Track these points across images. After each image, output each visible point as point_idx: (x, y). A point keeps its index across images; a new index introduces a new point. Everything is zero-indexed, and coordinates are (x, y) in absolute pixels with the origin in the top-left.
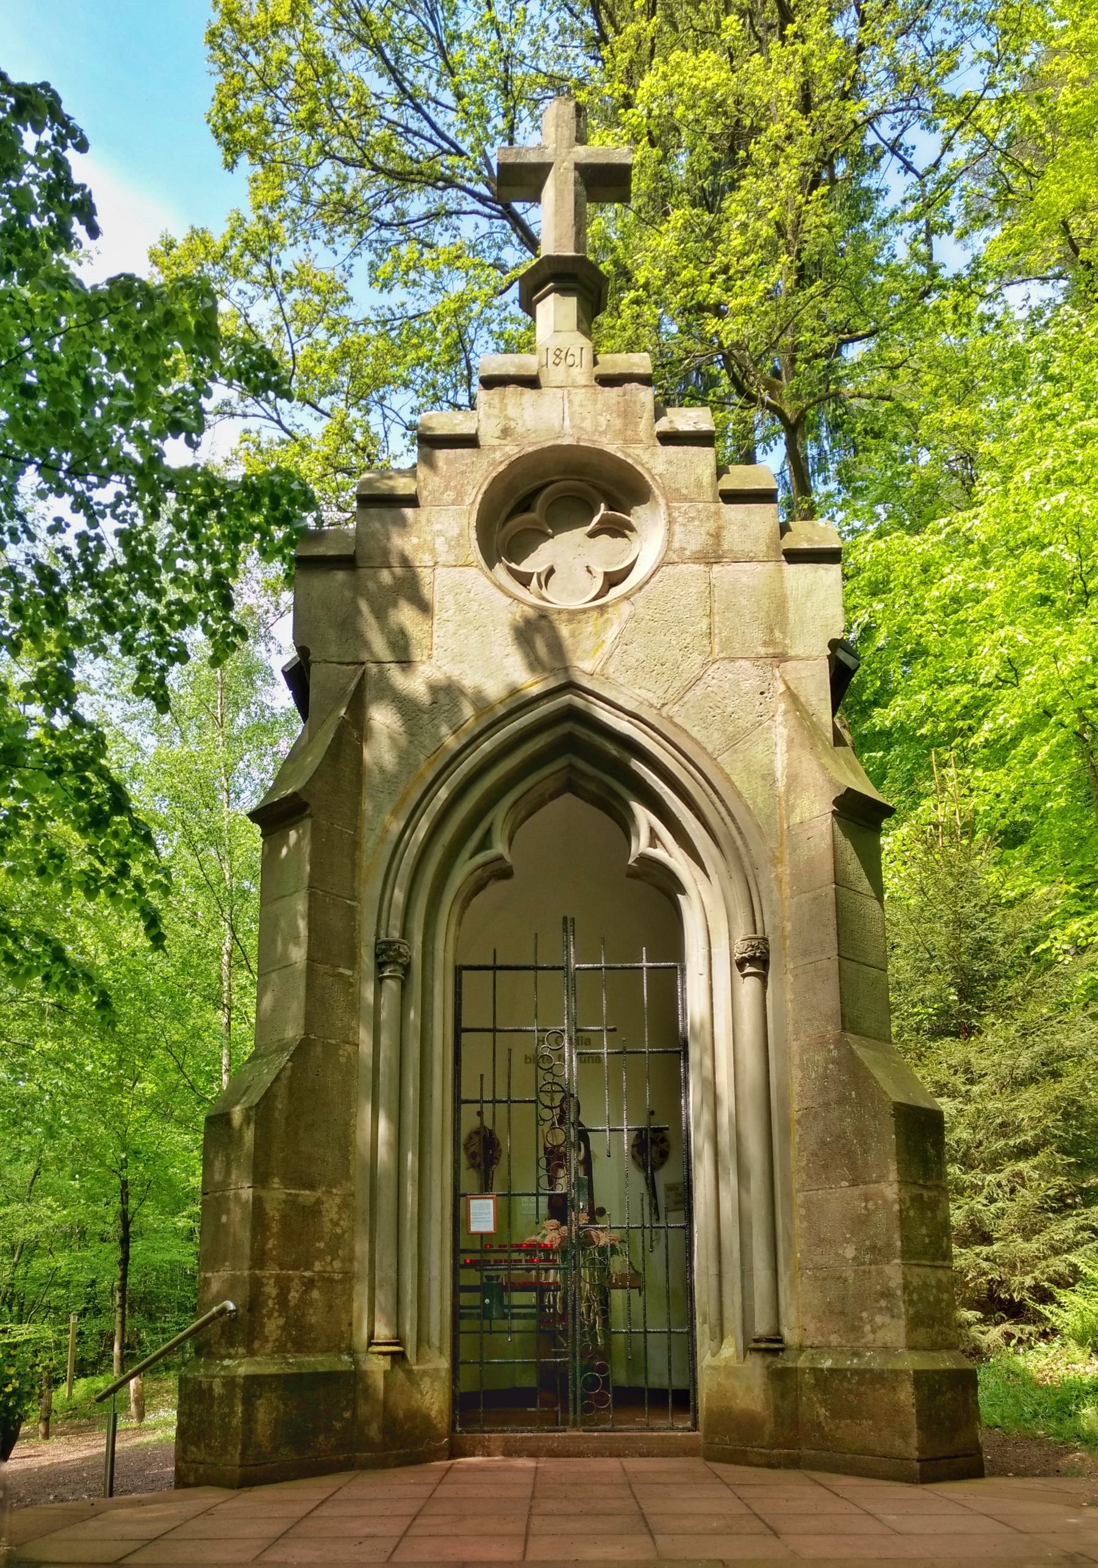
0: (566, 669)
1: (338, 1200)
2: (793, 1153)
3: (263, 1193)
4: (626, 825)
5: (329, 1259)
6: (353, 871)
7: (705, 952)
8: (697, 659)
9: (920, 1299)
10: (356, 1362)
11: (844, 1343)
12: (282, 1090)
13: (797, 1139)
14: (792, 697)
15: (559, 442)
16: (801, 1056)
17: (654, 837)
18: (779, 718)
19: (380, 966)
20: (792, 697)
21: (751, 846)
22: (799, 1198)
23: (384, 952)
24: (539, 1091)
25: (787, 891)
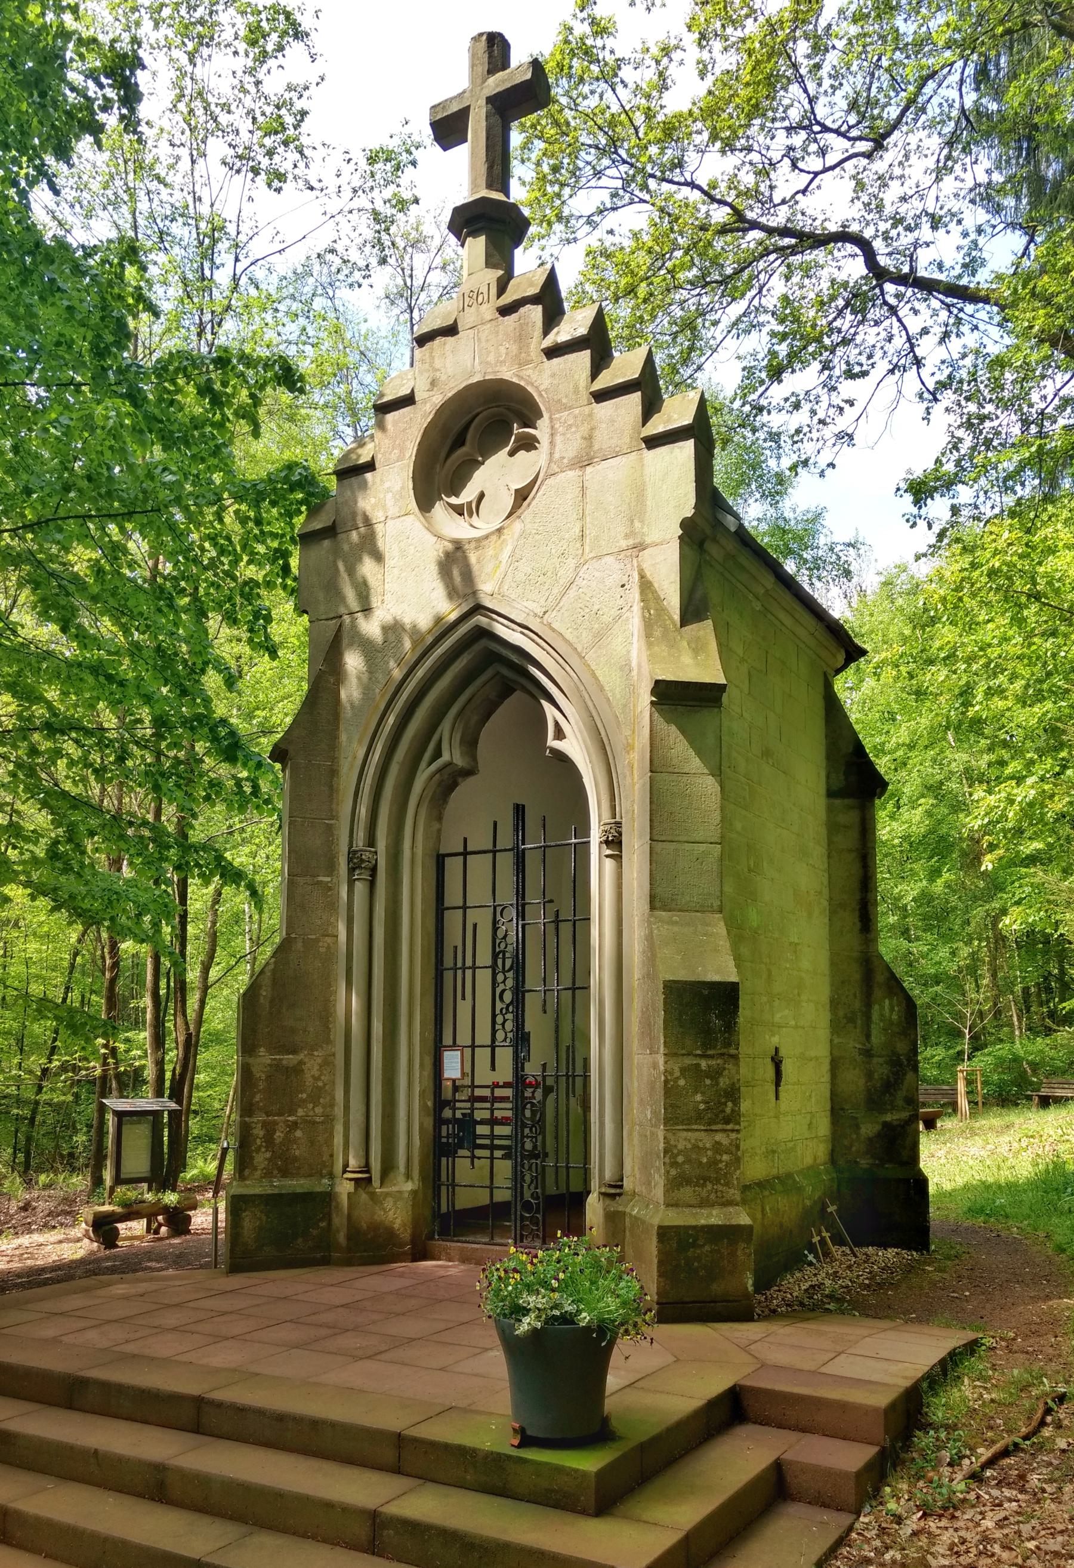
0: (475, 593)
1: (319, 1061)
3: (251, 1061)
5: (311, 1106)
6: (331, 796)
8: (571, 563)
9: (688, 1161)
10: (332, 1186)
12: (266, 980)
14: (646, 585)
15: (470, 382)
19: (351, 871)
20: (646, 585)
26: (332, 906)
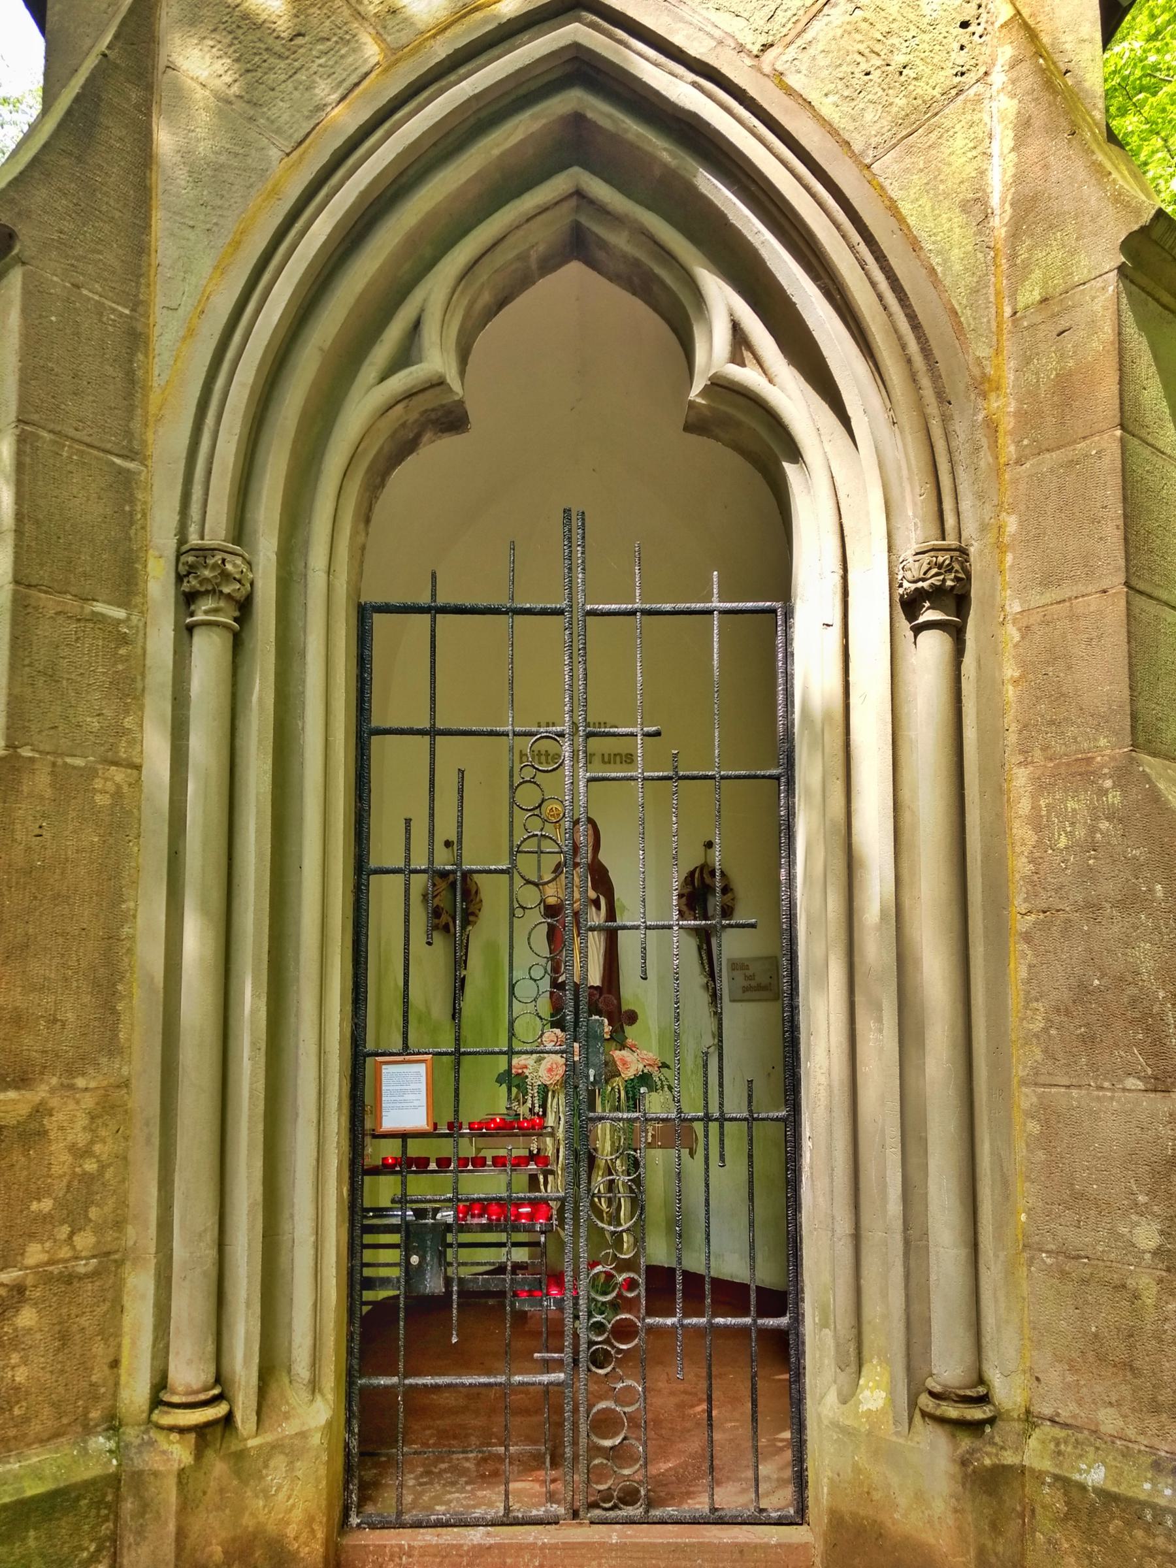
1: (88, 1101)
2: (1015, 999)
4: (680, 319)
5: (65, 1230)
6: (129, 395)
7: (837, 579)
11: (1131, 1432)
13: (1023, 973)
16: (1035, 798)
17: (740, 340)
18: (998, 78)
19: (188, 599)
21: (937, 354)
22: (1026, 1098)
23: (192, 569)
24: (515, 852)
25: (1010, 450)
26: (127, 689)
